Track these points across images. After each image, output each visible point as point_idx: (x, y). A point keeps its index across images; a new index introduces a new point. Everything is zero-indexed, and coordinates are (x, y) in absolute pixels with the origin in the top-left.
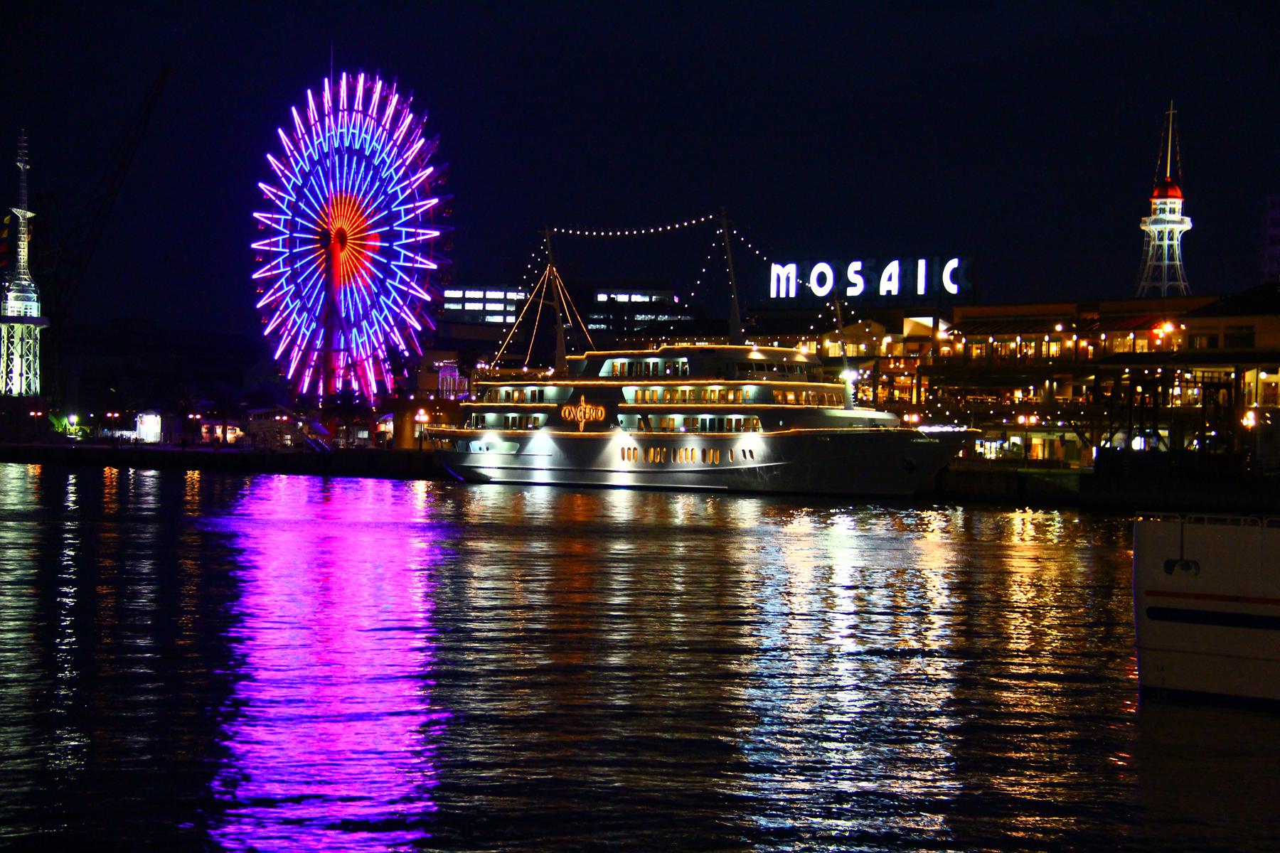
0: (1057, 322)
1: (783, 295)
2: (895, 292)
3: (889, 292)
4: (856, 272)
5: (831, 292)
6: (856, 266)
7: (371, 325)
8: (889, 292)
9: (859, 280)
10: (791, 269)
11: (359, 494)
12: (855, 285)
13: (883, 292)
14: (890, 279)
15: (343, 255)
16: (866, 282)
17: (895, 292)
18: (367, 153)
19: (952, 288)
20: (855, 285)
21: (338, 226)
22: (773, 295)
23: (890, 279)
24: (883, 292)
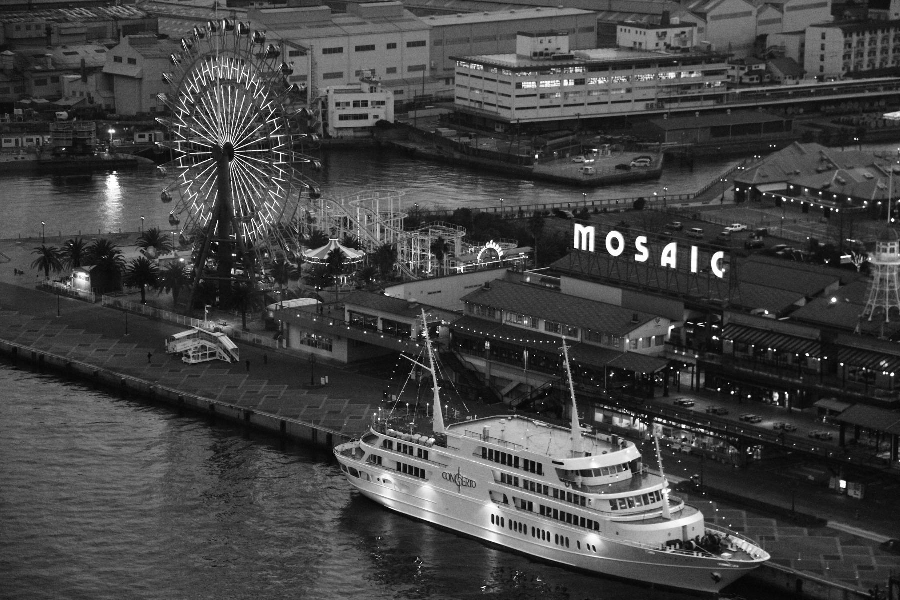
0: (834, 306)
1: (584, 248)
2: (673, 266)
3: (669, 265)
4: (643, 244)
5: (625, 251)
6: (641, 240)
7: (199, 81)
8: (669, 265)
9: (645, 251)
10: (591, 230)
11: (358, 457)
12: (641, 254)
13: (664, 264)
14: (669, 255)
15: (232, 164)
16: (651, 253)
17: (673, 266)
18: (239, 82)
19: (719, 273)
20: (641, 254)
21: (227, 141)
22: (577, 246)
23: (669, 255)
24: (664, 264)
